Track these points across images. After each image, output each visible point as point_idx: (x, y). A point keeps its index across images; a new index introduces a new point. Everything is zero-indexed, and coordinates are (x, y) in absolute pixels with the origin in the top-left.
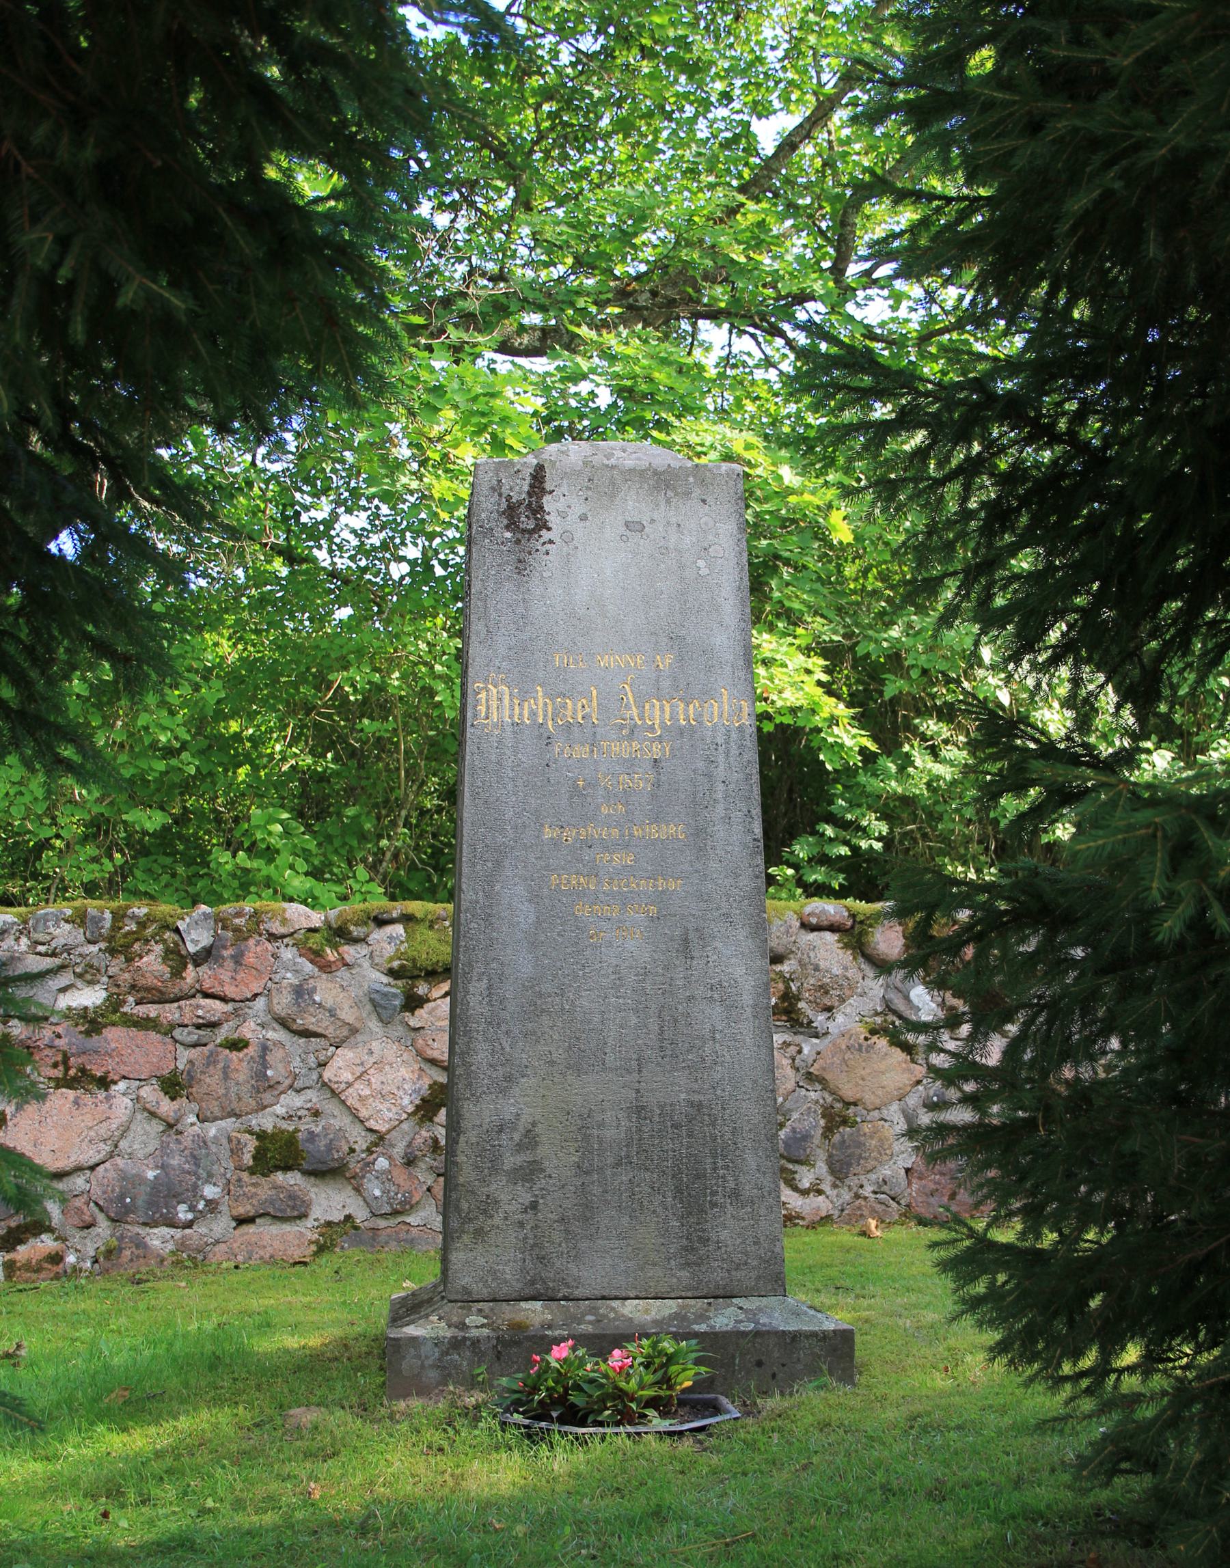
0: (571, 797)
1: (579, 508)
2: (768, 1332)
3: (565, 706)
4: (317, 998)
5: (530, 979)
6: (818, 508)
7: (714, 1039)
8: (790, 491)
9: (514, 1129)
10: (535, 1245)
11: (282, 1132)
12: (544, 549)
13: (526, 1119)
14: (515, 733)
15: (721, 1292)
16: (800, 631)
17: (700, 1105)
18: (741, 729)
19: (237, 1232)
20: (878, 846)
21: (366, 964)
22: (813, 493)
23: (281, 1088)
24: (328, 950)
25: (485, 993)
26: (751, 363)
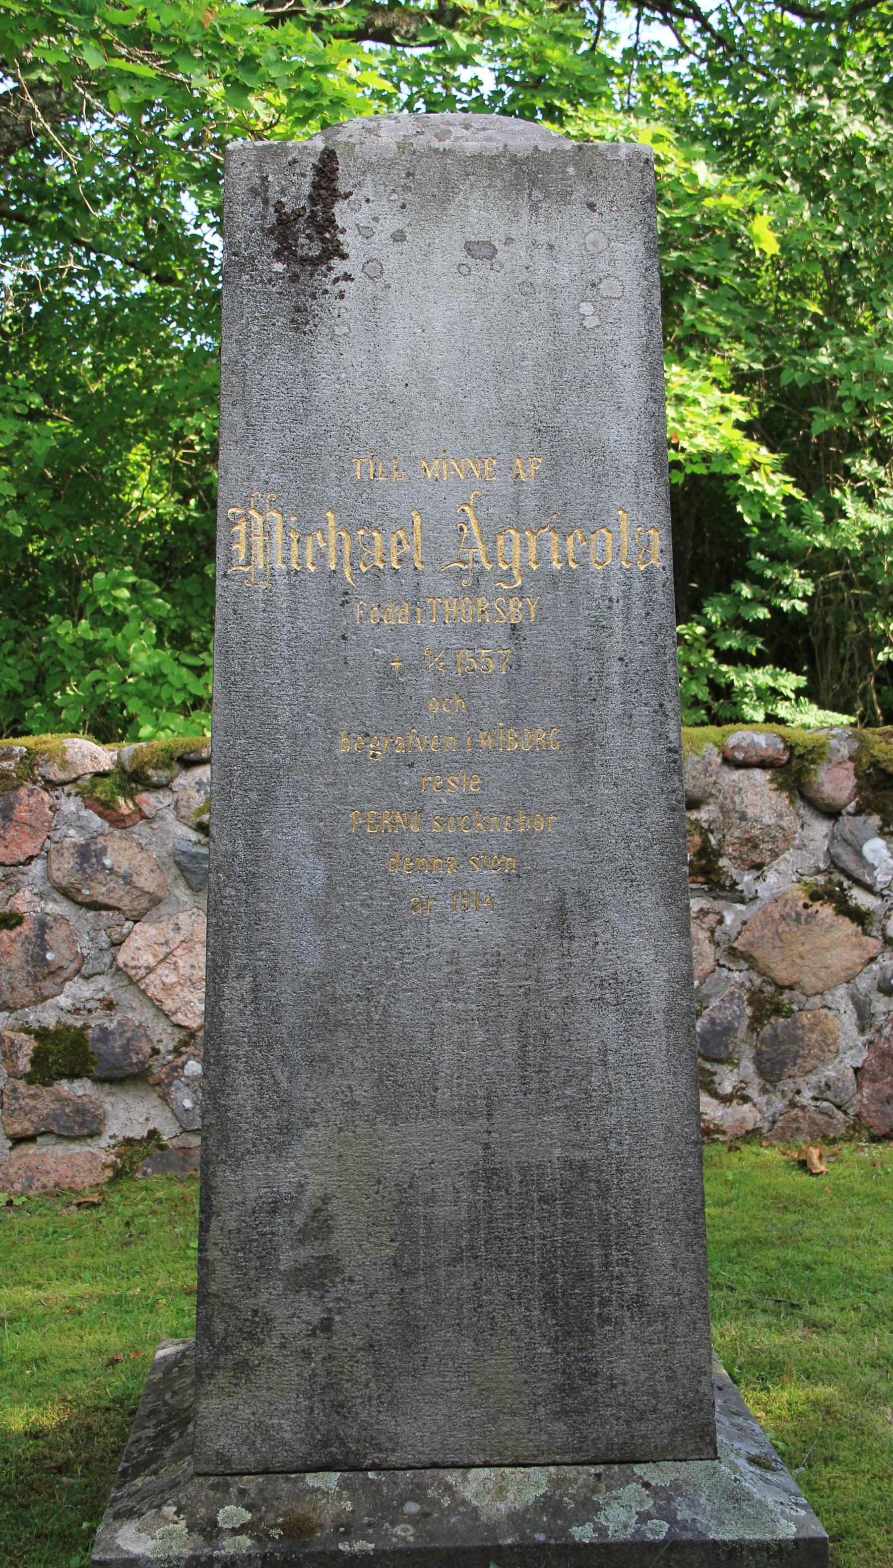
0: (382, 687)
1: (391, 223)
2: (690, 1544)
3: (369, 542)
4: (108, 862)
5: (318, 975)
6: (738, 212)
7: (605, 1063)
8: (705, 193)
9: (294, 1207)
10: (330, 1386)
11: (68, 1028)
12: (336, 289)
13: (312, 1191)
14: (292, 586)
15: (616, 1455)
16: (715, 360)
17: (584, 1167)
18: (648, 575)
19: (14, 1153)
20: (801, 606)
21: (170, 816)
22: (733, 193)
23: (65, 974)
24: (121, 801)
25: (249, 997)
26: (660, 54)
